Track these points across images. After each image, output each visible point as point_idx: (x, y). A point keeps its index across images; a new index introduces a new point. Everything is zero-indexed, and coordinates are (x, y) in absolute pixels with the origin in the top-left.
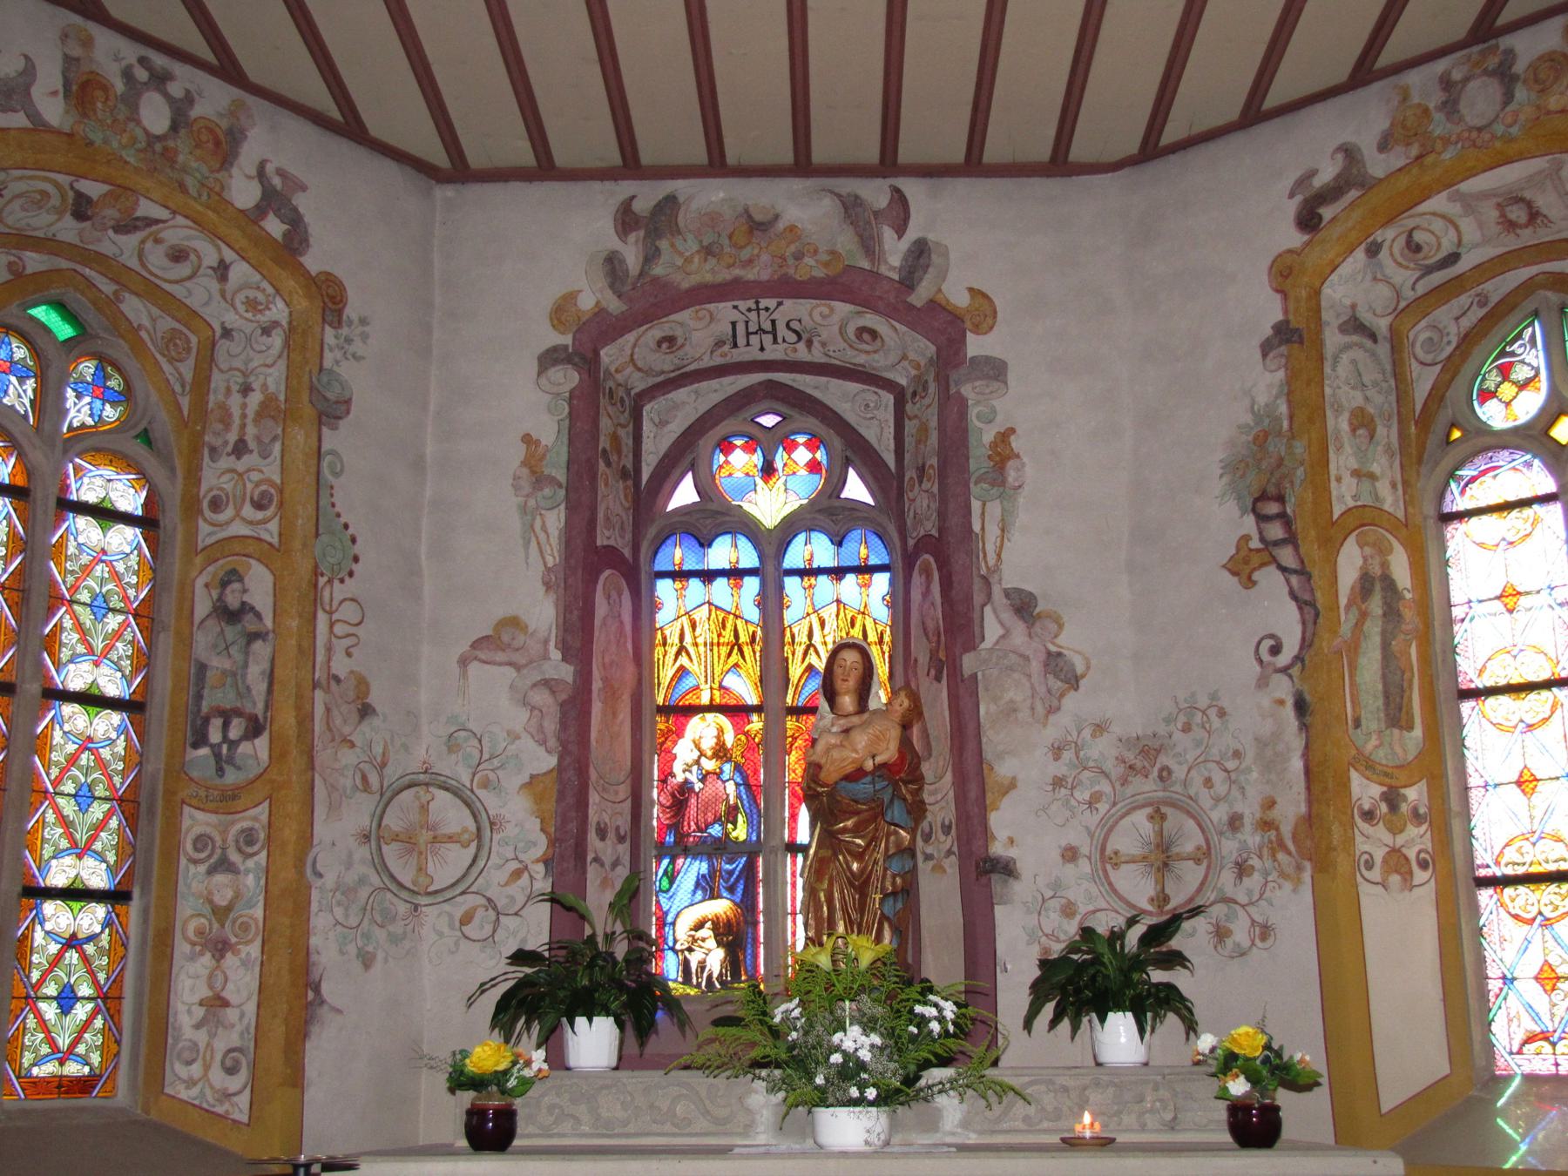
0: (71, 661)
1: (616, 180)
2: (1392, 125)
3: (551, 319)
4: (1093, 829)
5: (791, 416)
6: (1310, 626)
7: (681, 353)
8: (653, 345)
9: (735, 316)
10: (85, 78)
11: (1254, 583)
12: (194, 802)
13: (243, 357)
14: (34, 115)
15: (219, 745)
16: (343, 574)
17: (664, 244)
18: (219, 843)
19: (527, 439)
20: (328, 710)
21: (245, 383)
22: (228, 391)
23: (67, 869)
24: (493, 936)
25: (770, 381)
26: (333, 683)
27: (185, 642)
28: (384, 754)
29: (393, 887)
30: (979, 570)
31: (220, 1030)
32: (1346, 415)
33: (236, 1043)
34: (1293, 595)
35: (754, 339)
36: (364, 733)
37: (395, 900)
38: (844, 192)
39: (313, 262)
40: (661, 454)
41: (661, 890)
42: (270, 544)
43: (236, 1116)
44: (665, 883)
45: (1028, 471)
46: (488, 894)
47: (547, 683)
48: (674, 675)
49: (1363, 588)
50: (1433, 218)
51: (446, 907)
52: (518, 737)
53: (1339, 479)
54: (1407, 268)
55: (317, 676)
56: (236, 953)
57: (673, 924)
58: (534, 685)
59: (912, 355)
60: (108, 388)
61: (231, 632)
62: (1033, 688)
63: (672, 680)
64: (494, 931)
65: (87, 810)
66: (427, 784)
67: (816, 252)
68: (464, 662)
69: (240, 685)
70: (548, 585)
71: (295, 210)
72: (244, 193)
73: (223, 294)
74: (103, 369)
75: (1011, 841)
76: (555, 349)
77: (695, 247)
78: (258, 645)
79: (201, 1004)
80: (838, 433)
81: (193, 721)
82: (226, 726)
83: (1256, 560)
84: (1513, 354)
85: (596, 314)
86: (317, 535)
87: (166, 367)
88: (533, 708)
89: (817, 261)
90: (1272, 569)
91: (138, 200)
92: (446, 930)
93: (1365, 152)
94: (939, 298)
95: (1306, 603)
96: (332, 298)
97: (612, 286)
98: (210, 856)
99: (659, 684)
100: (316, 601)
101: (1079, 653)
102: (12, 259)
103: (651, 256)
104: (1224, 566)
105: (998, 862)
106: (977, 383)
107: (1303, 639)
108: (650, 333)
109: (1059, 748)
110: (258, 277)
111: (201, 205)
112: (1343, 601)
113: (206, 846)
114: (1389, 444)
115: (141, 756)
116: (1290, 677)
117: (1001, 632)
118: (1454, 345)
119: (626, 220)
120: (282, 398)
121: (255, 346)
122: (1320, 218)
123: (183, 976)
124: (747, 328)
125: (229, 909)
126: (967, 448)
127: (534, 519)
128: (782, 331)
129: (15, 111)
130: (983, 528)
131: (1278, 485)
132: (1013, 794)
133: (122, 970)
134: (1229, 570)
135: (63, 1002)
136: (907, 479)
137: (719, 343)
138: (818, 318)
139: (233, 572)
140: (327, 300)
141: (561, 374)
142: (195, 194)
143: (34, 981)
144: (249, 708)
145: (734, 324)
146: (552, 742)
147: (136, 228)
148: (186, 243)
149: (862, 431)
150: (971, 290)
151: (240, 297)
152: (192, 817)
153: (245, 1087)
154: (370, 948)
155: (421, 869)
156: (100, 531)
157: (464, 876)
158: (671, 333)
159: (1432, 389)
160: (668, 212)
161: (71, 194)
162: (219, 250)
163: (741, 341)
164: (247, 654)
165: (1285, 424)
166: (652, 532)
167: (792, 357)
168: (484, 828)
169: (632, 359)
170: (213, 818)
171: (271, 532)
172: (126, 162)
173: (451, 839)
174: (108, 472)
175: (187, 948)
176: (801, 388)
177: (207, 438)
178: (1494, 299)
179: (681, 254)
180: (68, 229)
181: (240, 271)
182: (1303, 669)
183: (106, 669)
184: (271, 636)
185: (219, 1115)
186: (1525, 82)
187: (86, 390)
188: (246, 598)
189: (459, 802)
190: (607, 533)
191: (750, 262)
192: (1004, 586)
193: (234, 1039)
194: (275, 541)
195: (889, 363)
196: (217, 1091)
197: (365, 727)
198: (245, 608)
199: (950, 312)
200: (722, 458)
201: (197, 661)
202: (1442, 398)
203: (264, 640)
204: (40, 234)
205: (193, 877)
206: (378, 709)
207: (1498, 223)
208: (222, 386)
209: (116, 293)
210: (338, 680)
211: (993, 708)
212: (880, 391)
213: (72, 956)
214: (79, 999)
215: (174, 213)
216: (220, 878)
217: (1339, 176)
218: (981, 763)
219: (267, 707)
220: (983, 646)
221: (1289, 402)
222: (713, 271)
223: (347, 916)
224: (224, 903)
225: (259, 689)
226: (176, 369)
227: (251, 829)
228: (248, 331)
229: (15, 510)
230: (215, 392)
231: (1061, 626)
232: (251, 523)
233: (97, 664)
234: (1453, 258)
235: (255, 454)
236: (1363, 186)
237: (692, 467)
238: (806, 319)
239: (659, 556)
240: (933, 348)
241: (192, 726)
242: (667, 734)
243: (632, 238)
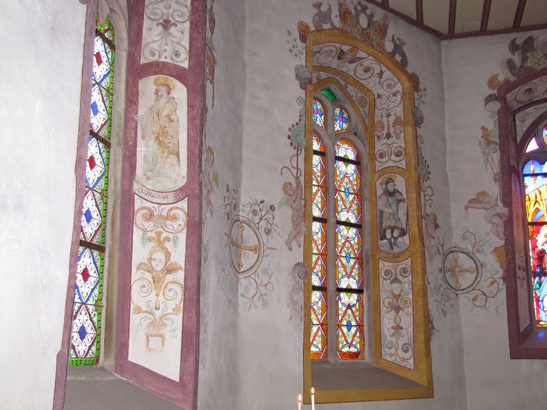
0: (341, 211)
7: (533, 94)
8: (523, 92)
10: (344, 10)
12: (383, 259)
13: (386, 104)
14: (332, 24)
15: (391, 239)
16: (426, 178)
17: (529, 55)
18: (394, 273)
19: (483, 128)
20: (426, 226)
21: (388, 113)
22: (382, 116)
23: (345, 282)
24: (485, 305)
26: (427, 216)
27: (374, 204)
28: (443, 241)
29: (450, 288)
31: (400, 337)
33: (406, 342)
36: (437, 233)
37: (451, 292)
39: (410, 69)
41: (536, 289)
42: (403, 169)
43: (409, 367)
44: (538, 286)
46: (482, 290)
47: (498, 215)
48: (534, 211)
51: (467, 295)
52: (489, 234)
55: (422, 214)
56: (404, 311)
57: (542, 301)
58: (493, 216)
60: (344, 117)
61: (391, 200)
63: (533, 213)
64: (486, 303)
65: (349, 262)
66: (456, 252)
68: (466, 208)
69: (396, 218)
70: (495, 180)
71: (403, 51)
72: (389, 47)
73: (380, 83)
74: (342, 111)
76: (491, 96)
77: (542, 55)
78: (401, 204)
79: (392, 328)
81: (380, 231)
82: (392, 232)
85: (505, 82)
86: (418, 165)
87: (361, 109)
88: (493, 224)
91: (358, 51)
92: (468, 303)
96: (416, 82)
97: (510, 71)
98: (391, 277)
99: (529, 215)
100: (420, 188)
102: (317, 75)
108: (523, 88)
110: (393, 76)
111: (377, 51)
113: (389, 274)
115: (362, 243)
119: (514, 47)
120: (402, 117)
121: (391, 100)
123: (385, 319)
125: (399, 295)
127: (488, 156)
129: (327, 23)
133: (363, 316)
135: (348, 327)
139: (390, 178)
140: (414, 82)
142: (376, 48)
143: (340, 320)
144: (400, 226)
146: (502, 236)
147: (356, 61)
148: (370, 65)
151: (385, 84)
152: (383, 264)
153: (411, 357)
154: (445, 309)
155: (457, 281)
156: (345, 166)
157: (473, 284)
161: (339, 50)
162: (381, 67)
164: (398, 207)
166: (522, 160)
168: (479, 267)
170: (391, 264)
171: (403, 164)
172: (357, 38)
173: (467, 271)
174: (346, 146)
175: (386, 309)
177: (375, 133)
179: (536, 58)
180: (334, 63)
181: (387, 74)
183: (350, 214)
184: (406, 200)
185: (402, 366)
187: (338, 118)
188: (395, 188)
189: (468, 257)
193: (405, 340)
194: (405, 167)
196: (401, 358)
197: (437, 231)
198: (396, 191)
201: (379, 210)
203: (403, 202)
204: (326, 65)
205: (385, 285)
206: (440, 226)
208: (380, 115)
209: (345, 84)
210: (427, 215)
213: (349, 311)
214: (352, 326)
215: (369, 55)
216: (395, 285)
219: (407, 225)
223: (438, 298)
224: (398, 294)
225: (403, 219)
226: (363, 110)
227: (405, 268)
228: (387, 95)
229: (322, 160)
230: (377, 117)
232: (395, 161)
233: (348, 212)
235: (394, 137)
237: (535, 136)
239: (524, 169)
241: (380, 233)
242: (533, 232)
243: (516, 53)
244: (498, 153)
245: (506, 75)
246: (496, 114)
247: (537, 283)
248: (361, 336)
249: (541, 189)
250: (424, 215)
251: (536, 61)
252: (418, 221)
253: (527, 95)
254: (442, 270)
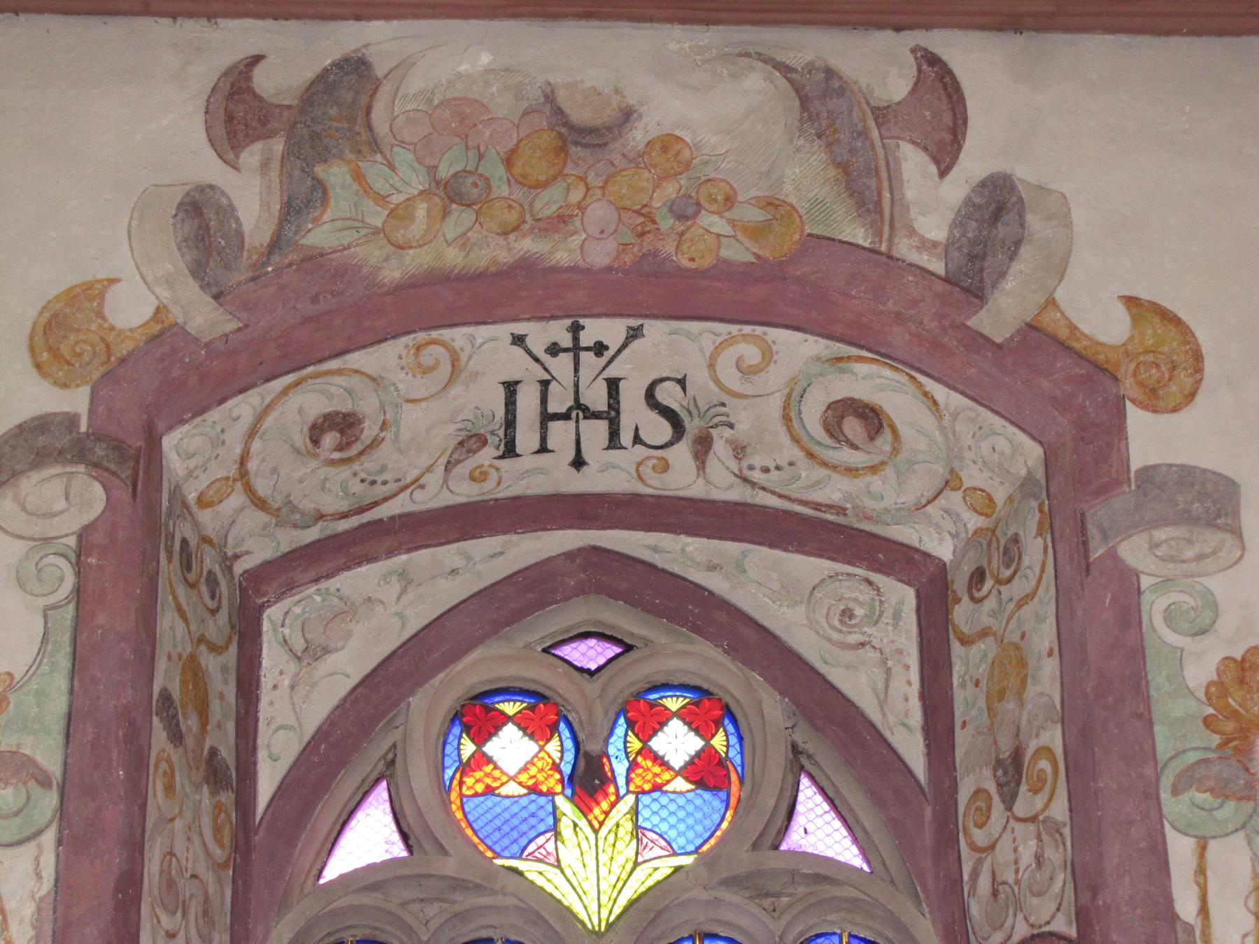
1: (211, 17)
3: (32, 349)
5: (647, 642)
7: (368, 465)
8: (300, 438)
9: (517, 365)
17: (335, 174)
25: (595, 549)
35: (561, 433)
38: (797, 59)
40: (310, 730)
59: (973, 476)
67: (730, 200)
76: (42, 424)
77: (417, 182)
80: (772, 681)
85: (154, 339)
89: (732, 222)
94: (1050, 320)
97: (198, 271)
106: (1160, 534)
108: (296, 400)
124: (544, 401)
126: (1147, 700)
128: (634, 411)
130: (1204, 911)
136: (963, 797)
137: (471, 442)
138: (731, 378)
141: (57, 487)
145: (511, 388)
149: (837, 677)
150: (1131, 302)
158: (347, 407)
160: (349, 97)
163: (526, 438)
167: (655, 485)
169: (243, 473)
176: (676, 569)
179: (381, 199)
190: (167, 922)
191: (561, 221)
195: (909, 498)
199: (1080, 356)
200: (468, 748)
212: (876, 577)
222: (463, 241)
237: (389, 771)
238: (699, 378)
240: (1035, 451)
243: (252, 155)
244: (40, 847)
245: (164, 294)
246: (63, 563)
251: (377, 217)
253: (333, 463)
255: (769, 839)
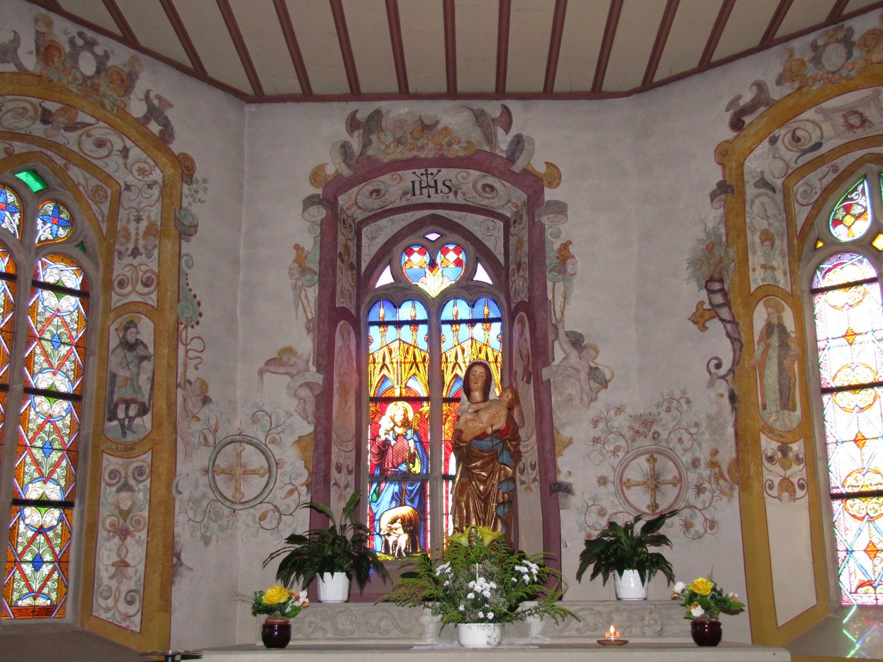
0: (40, 372)
1: (347, 101)
2: (784, 70)
3: (310, 180)
4: (615, 466)
5: (446, 234)
6: (738, 352)
7: (383, 199)
8: (368, 194)
9: (414, 178)
10: (48, 44)
11: (706, 328)
12: (109, 451)
13: (137, 201)
14: (19, 65)
15: (124, 420)
16: (193, 323)
17: (374, 138)
18: (123, 474)
19: (297, 247)
20: (185, 400)
21: (138, 216)
22: (129, 220)
23: (38, 489)
24: (277, 527)
25: (434, 214)
26: (187, 385)
27: (104, 361)
28: (216, 424)
29: (221, 499)
30: (551, 321)
31: (124, 580)
32: (758, 234)
33: (133, 587)
34: (728, 335)
35: (425, 191)
36: (205, 412)
37: (222, 507)
38: (475, 108)
39: (176, 147)
40: (372, 255)
41: (372, 501)
42: (152, 306)
43: (133, 628)
44: (375, 497)
45: (579, 265)
46: (275, 503)
47: (308, 385)
48: (380, 380)
49: (767, 331)
50: (807, 123)
51: (251, 510)
52: (292, 415)
53: (754, 270)
54: (792, 151)
55: (178, 381)
56: (133, 536)
57: (379, 520)
58: (301, 386)
59: (513, 200)
60: (61, 218)
61: (130, 356)
62: (581, 387)
63: (378, 383)
64: (278, 524)
65: (49, 456)
66: (240, 442)
67: (459, 142)
68: (261, 373)
69: (135, 385)
70: (308, 330)
71: (166, 118)
72: (138, 109)
73: (125, 165)
74: (58, 208)
75: (570, 473)
76: (312, 197)
77: (392, 139)
78: (145, 363)
79: (113, 565)
80: (472, 244)
81: (109, 406)
82: (127, 409)
83: (707, 315)
84: (852, 199)
85: (336, 177)
86: (179, 301)
87: (94, 207)
88: (300, 399)
89: (460, 147)
90: (716, 320)
91: (78, 112)
92: (251, 524)
93: (769, 85)
94: (529, 168)
95: (736, 339)
97: (345, 161)
98: (118, 482)
99: (371, 385)
100: (178, 338)
101: (608, 367)
102: (7, 146)
103: (366, 144)
104: (689, 319)
105: (562, 485)
106: (550, 216)
107: (734, 360)
108: (366, 188)
109: (596, 421)
110: (145, 156)
111: (113, 115)
112: (756, 338)
113: (116, 476)
114: (782, 250)
115: (80, 425)
116: (727, 381)
117: (564, 356)
118: (819, 194)
119: (353, 124)
120: (159, 224)
121: (143, 195)
122: (744, 123)
123: (103, 550)
124: (421, 185)
125: (129, 511)
126: (545, 252)
127: (301, 292)
128: (440, 186)
129: (8, 62)
130: (553, 298)
131: (720, 273)
132: (570, 447)
133: (69, 546)
134: (692, 321)
135: (36, 564)
136: (511, 269)
137: (405, 193)
138: (460, 179)
139: (131, 322)
140: (184, 169)
141: (316, 211)
143: (19, 552)
144: (140, 399)
145: (413, 182)
146: (311, 418)
147: (77, 128)
148: (105, 137)
149: (486, 243)
150: (547, 163)
151: (135, 167)
152: (108, 460)
153: (138, 612)
154: (208, 534)
155: (237, 489)
156: (56, 299)
157: (261, 493)
158: (378, 188)
159: (807, 219)
160: (376, 119)
161: (40, 109)
162: (123, 141)
163: (417, 192)
164: (139, 368)
165: (724, 239)
166: (367, 299)
167: (446, 201)
168: (272, 466)
169: (356, 202)
170: (120, 461)
171: (153, 300)
173: (254, 472)
175: (105, 534)
176: (451, 219)
177: (116, 247)
178: (841, 168)
179: (383, 143)
181: (135, 153)
182: (734, 377)
183: (60, 377)
184: (153, 358)
185: (123, 628)
186: (859, 46)
187: (49, 219)
188: (139, 337)
189: (258, 451)
190: (342, 300)
191: (422, 147)
192: (566, 330)
193: (132, 585)
194: (155, 304)
195: (501, 204)
196: (122, 614)
197: (206, 409)
198: (138, 342)
199: (535, 176)
200: (407, 258)
201: (111, 372)
202: (812, 224)
203: (149, 360)
204: (23, 132)
205: (109, 494)
206: (213, 399)
207: (844, 126)
208: (125, 217)
209: (65, 165)
210: (190, 383)
211: (559, 398)
212: (495, 220)
213: (41, 538)
214: (44, 562)
215: (98, 120)
216: (124, 494)
217: (754, 99)
218: (553, 430)
219: (150, 398)
220: (553, 364)
221: (726, 226)
222: (401, 153)
223: (195, 516)
224: (126, 509)
225: (146, 388)
226: (99, 208)
227: (142, 467)
228: (140, 186)
229: (8, 287)
230: (121, 221)
231: (597, 353)
232: (141, 294)
233: (54, 374)
234: (818, 145)
235: (144, 255)
236: (767, 105)
237: (390, 263)
238: (454, 180)
239: (371, 313)
240: (526, 196)
241: (108, 409)
242: (376, 413)
243: (356, 134)
247: (375, 491)
248: (62, 579)
249: (392, 346)
250: (182, 384)
252: (168, 392)
254: (210, 471)
255: (470, 278)
